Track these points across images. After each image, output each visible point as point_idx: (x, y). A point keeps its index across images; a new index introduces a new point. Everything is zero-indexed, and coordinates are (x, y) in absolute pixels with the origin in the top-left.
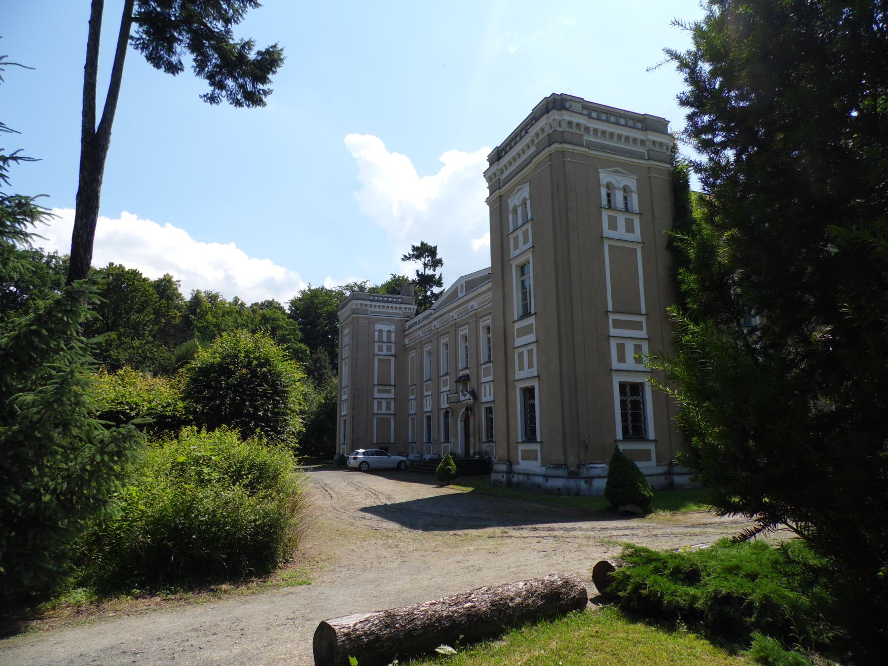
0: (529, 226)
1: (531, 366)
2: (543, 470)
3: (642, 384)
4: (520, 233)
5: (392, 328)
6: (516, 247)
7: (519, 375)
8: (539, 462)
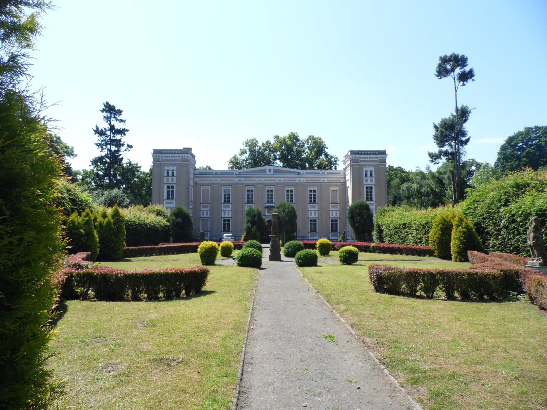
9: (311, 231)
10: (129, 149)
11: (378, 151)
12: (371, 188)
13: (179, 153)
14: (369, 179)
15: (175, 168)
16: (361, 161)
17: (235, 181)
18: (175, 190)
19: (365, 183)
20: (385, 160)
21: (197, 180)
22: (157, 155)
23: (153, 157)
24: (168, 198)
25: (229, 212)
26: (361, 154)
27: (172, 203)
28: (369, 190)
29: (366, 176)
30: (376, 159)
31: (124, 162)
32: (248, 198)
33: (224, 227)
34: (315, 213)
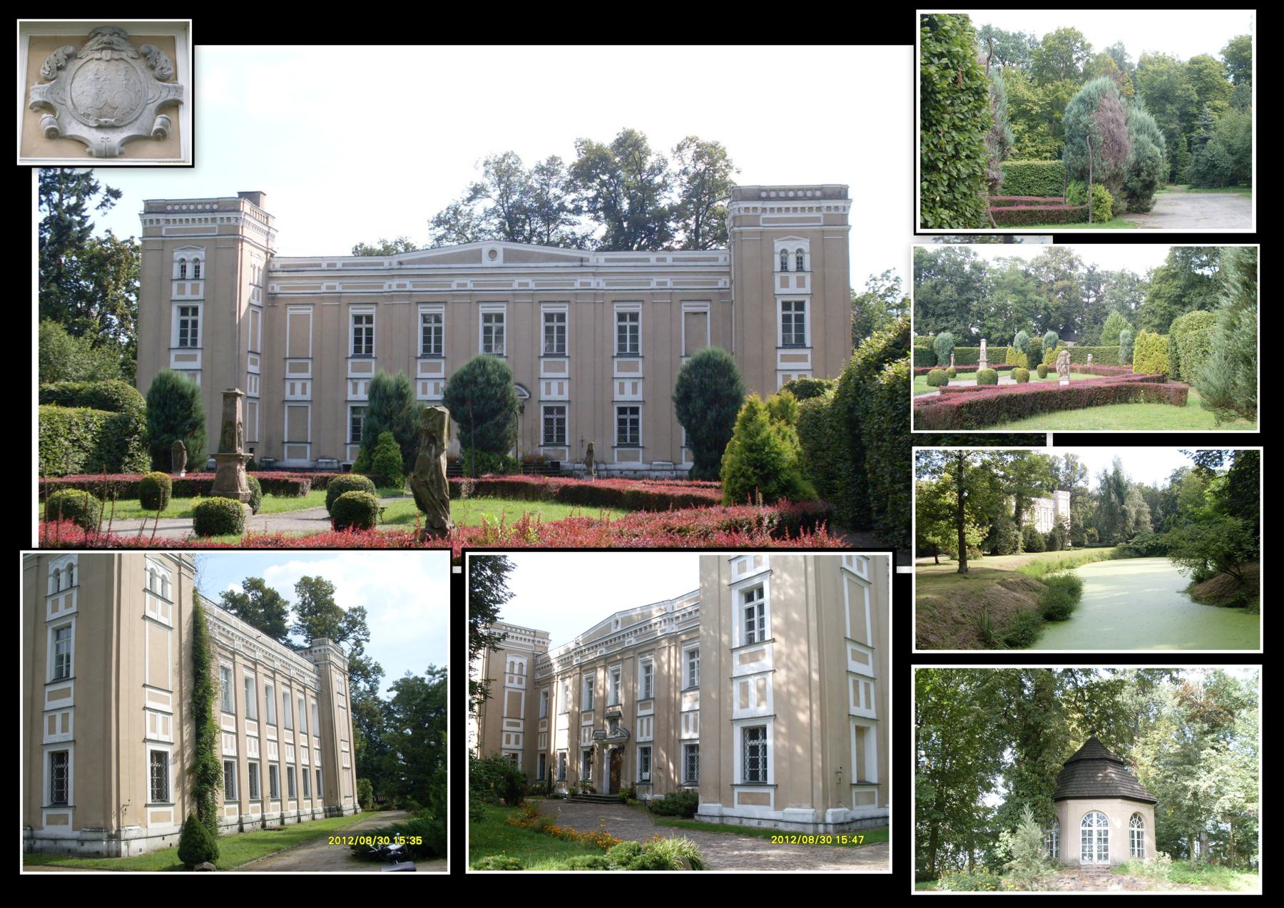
0: (75, 593)
1: (65, 729)
2: (77, 834)
3: (166, 754)
4: (62, 598)
5: (524, 661)
6: (55, 610)
7: (48, 739)
8: (172, 823)
9: (622, 442)
10: (113, 200)
11: (821, 188)
12: (800, 306)
13: (213, 211)
14: (793, 279)
15: (201, 255)
16: (766, 220)
17: (386, 288)
18: (200, 318)
19: (778, 290)
20: (845, 217)
21: (277, 290)
22: (154, 217)
23: (144, 222)
24: (183, 343)
25: (304, 386)
26: (768, 199)
27: (194, 358)
28: (793, 313)
29: (784, 268)
30: (815, 214)
31: (97, 233)
32: (427, 340)
33: (548, 431)
34: (635, 386)
